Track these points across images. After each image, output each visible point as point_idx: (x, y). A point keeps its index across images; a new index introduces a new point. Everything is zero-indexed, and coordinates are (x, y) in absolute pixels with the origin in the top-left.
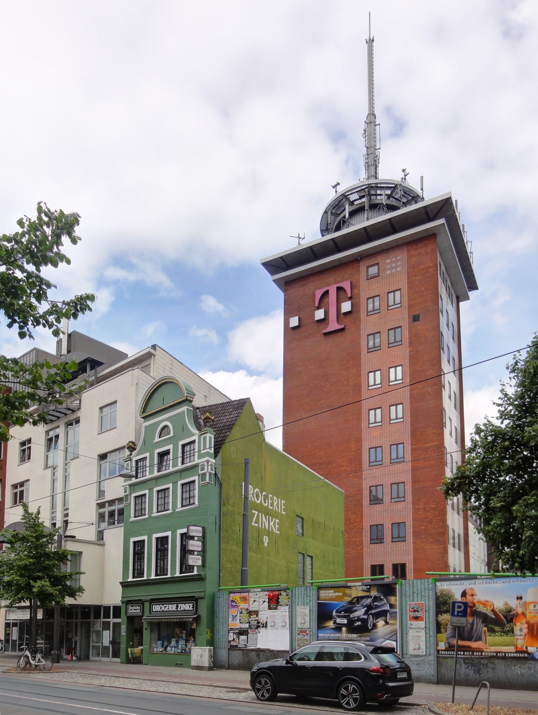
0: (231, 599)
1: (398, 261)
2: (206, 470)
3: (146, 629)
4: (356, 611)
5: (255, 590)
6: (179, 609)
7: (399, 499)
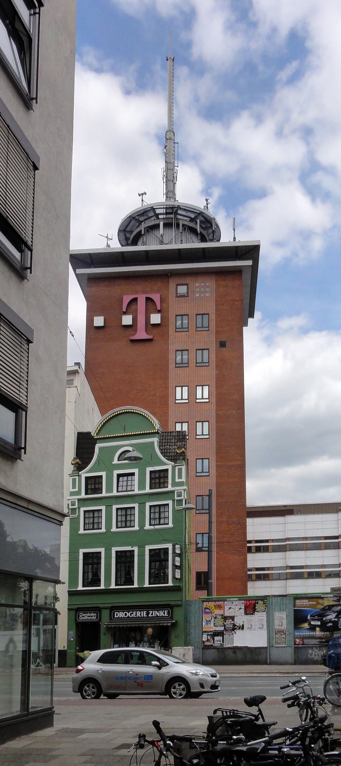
0: (205, 606)
1: (208, 287)
2: (182, 498)
3: (105, 634)
4: (328, 615)
5: (231, 599)
6: (150, 615)
7: (204, 511)
